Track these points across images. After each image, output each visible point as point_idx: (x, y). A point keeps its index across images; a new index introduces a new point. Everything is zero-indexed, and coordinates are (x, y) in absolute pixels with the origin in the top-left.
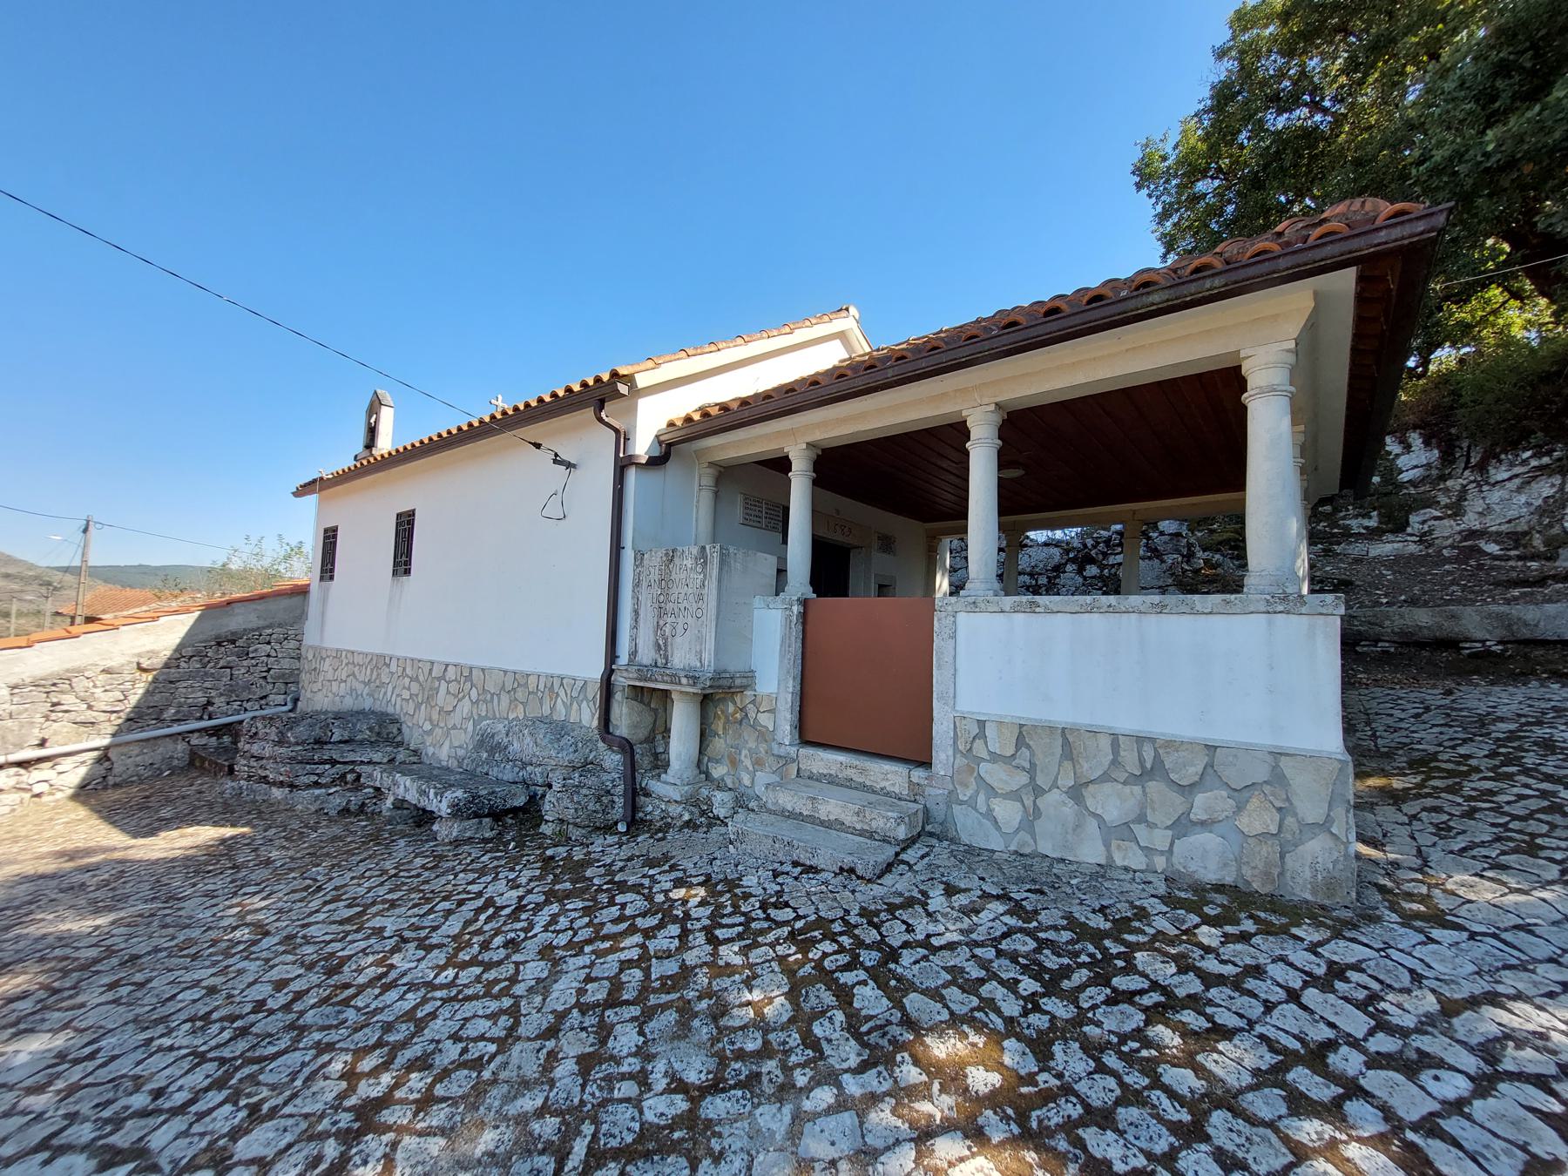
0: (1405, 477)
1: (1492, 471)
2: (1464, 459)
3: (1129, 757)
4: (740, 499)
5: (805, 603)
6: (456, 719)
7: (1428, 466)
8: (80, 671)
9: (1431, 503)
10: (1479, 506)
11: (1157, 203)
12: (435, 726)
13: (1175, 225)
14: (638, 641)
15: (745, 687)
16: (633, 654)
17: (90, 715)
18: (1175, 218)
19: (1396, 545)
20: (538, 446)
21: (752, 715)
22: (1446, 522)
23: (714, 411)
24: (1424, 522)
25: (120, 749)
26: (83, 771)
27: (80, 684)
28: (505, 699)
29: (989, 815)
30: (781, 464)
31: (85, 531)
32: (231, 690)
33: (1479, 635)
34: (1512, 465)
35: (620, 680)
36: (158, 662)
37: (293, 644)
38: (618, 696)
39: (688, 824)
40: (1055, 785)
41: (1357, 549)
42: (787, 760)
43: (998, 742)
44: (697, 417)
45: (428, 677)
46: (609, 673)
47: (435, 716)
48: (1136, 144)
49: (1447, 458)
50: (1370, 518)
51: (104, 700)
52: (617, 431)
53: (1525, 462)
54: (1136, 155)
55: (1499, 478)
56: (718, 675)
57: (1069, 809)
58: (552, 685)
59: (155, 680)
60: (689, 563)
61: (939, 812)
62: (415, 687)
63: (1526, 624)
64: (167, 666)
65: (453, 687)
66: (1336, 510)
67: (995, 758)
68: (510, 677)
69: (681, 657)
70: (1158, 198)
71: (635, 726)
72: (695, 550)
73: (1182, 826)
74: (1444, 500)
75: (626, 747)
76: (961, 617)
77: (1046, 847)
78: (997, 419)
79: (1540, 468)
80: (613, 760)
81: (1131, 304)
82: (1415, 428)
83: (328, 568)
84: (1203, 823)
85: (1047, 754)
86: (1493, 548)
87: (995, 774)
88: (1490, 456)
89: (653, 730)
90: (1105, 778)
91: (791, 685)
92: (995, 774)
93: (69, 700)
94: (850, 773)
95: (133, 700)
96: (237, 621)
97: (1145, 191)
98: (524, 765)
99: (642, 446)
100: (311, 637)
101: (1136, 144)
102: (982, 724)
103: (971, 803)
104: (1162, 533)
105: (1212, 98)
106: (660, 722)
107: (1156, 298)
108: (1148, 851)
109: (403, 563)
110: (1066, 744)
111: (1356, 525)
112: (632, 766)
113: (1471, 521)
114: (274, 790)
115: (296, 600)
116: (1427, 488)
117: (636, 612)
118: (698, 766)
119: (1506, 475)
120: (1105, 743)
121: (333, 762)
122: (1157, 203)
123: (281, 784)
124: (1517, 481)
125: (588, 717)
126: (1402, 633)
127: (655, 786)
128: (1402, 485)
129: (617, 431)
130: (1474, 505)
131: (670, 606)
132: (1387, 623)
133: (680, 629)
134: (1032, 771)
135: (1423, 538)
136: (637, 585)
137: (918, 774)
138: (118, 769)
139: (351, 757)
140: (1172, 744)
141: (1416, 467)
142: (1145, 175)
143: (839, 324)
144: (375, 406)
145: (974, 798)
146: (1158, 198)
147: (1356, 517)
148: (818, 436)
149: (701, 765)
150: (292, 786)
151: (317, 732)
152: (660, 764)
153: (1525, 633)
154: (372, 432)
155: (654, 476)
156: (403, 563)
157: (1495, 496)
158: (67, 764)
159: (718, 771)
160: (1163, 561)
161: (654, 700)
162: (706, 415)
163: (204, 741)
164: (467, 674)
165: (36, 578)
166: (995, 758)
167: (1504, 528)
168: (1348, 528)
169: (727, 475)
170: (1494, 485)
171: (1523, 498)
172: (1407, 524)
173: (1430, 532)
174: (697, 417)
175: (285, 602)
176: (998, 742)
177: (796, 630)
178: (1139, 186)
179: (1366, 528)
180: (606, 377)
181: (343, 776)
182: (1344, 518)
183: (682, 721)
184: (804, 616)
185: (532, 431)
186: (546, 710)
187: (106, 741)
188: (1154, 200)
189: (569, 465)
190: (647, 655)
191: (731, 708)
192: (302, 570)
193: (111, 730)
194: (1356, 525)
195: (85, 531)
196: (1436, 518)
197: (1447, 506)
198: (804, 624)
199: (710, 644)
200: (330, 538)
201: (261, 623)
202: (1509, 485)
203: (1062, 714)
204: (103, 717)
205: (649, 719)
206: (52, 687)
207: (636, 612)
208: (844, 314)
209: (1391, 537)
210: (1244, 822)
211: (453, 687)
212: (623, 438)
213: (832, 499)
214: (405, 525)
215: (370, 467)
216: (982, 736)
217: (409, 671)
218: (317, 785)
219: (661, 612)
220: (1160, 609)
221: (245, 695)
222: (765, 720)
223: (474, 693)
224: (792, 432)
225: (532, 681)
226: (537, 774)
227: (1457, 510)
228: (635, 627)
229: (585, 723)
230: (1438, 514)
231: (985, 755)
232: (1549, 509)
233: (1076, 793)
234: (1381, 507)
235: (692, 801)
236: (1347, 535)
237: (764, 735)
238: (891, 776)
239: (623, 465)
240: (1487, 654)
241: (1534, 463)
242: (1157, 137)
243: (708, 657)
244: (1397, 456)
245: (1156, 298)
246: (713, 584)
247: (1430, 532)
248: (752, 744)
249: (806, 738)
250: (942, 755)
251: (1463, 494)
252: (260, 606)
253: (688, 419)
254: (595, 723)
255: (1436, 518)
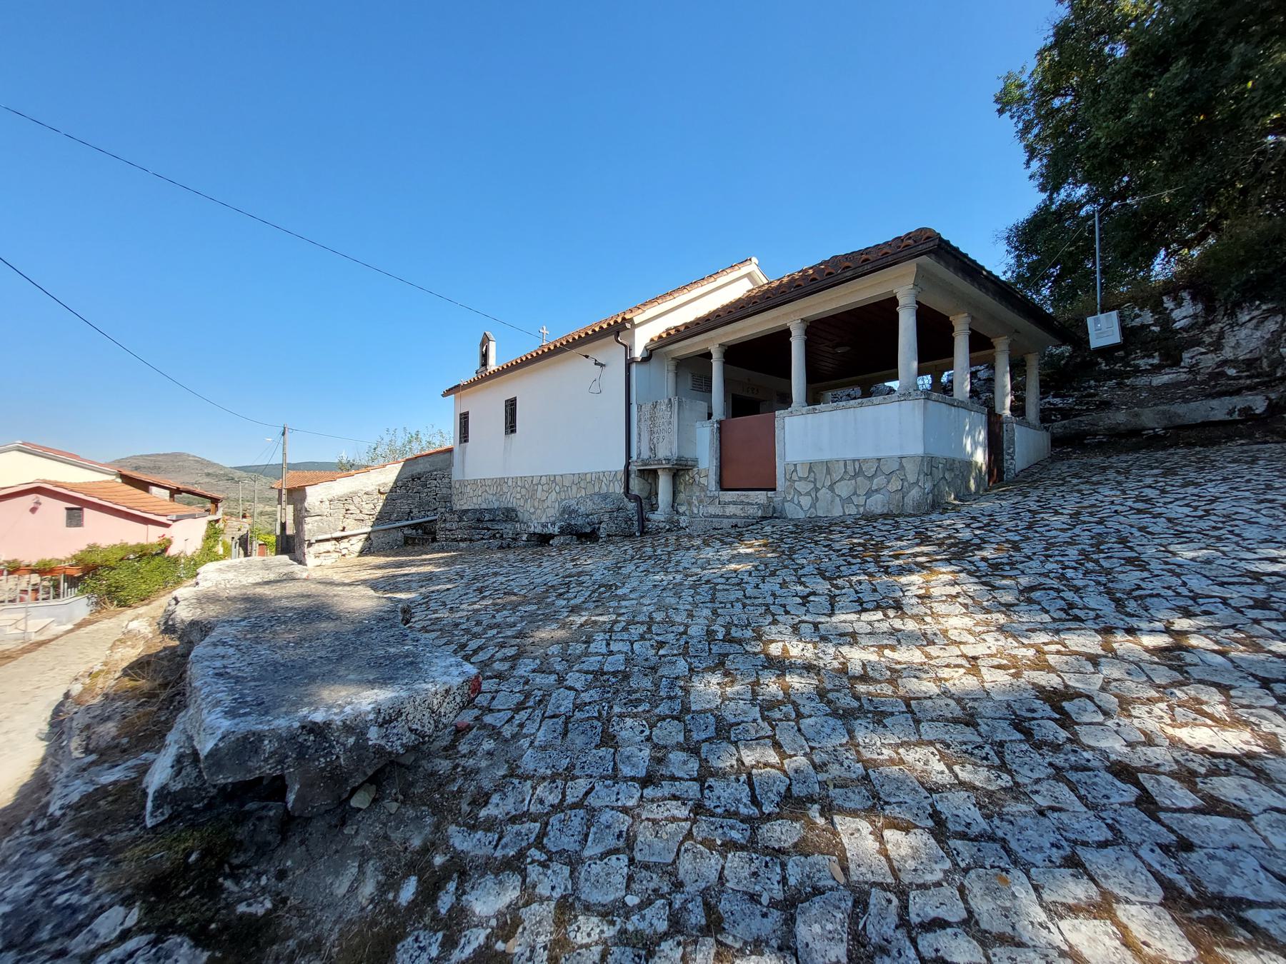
0: (1178, 325)
1: (1240, 316)
2: (1223, 308)
3: (850, 468)
4: (690, 375)
5: (720, 422)
6: (549, 503)
7: (1195, 316)
8: (356, 493)
9: (1199, 343)
10: (1232, 342)
11: (1018, 122)
12: (536, 509)
13: (1035, 136)
14: (641, 449)
15: (694, 466)
16: (639, 455)
17: (361, 516)
18: (1035, 131)
19: (1171, 376)
20: (587, 357)
21: (697, 479)
22: (1209, 356)
23: (673, 332)
24: (1192, 358)
25: (376, 534)
26: (361, 544)
27: (356, 500)
28: (574, 488)
29: (799, 504)
30: (708, 355)
31: (283, 434)
32: (420, 505)
33: (1151, 425)
34: (1250, 311)
35: (633, 468)
36: (387, 489)
37: (447, 480)
38: (633, 476)
39: (668, 530)
40: (823, 486)
41: (1142, 381)
42: (714, 498)
43: (802, 472)
44: (664, 335)
45: (530, 486)
46: (628, 465)
47: (536, 504)
48: (999, 78)
49: (1210, 310)
50: (1154, 357)
51: (367, 508)
52: (625, 346)
53: (1258, 308)
54: (998, 87)
55: (1244, 320)
56: (679, 459)
57: (830, 494)
58: (599, 477)
59: (387, 499)
60: (664, 407)
61: (779, 507)
62: (524, 491)
63: (1179, 416)
64: (391, 491)
65: (546, 488)
66: (1128, 354)
67: (801, 479)
68: (577, 476)
69: (662, 453)
70: (1019, 117)
71: (641, 490)
72: (666, 401)
73: (869, 494)
74: (1207, 340)
75: (637, 499)
76: (787, 419)
77: (820, 513)
78: (803, 326)
79: (1268, 310)
80: (632, 506)
81: (840, 277)
82: (1184, 288)
83: (464, 436)
84: (876, 490)
85: (820, 473)
86: (1232, 372)
87: (801, 486)
88: (1238, 305)
89: (650, 493)
90: (842, 479)
91: (715, 463)
92: (801, 486)
93: (352, 507)
94: (742, 498)
95: (379, 508)
96: (419, 468)
97: (1008, 114)
98: (588, 516)
99: (638, 353)
100: (456, 475)
101: (999, 78)
102: (795, 465)
103: (792, 501)
104: (980, 380)
105: (1054, 35)
106: (653, 490)
107: (848, 274)
108: (857, 506)
109: (511, 427)
110: (828, 468)
111: (1143, 363)
112: (641, 511)
113: (1228, 353)
114: (461, 544)
115: (447, 455)
116: (1197, 332)
117: (640, 434)
118: (673, 506)
119: (1247, 318)
120: (842, 464)
121: (489, 529)
122: (1018, 122)
123: (465, 540)
124: (1254, 321)
125: (619, 489)
126: (1109, 429)
127: (652, 516)
128: (1177, 331)
129: (625, 346)
130: (1230, 341)
131: (655, 429)
132: (1101, 423)
133: (661, 440)
134: (815, 482)
135: (1192, 369)
136: (639, 421)
137: (770, 493)
138: (375, 544)
139: (496, 527)
140: (866, 460)
141: (1185, 317)
142: (1004, 103)
143: (745, 269)
144: (485, 341)
145: (793, 498)
146: (1019, 117)
147: (1143, 358)
148: (724, 340)
149: (674, 504)
150: (471, 540)
151: (478, 515)
152: (654, 508)
153: (1179, 421)
154: (485, 356)
155: (645, 367)
156: (511, 427)
157: (1243, 333)
158: (354, 540)
159: (682, 509)
160: (979, 399)
161: (650, 475)
162: (669, 334)
163: (410, 532)
164: (553, 480)
165: (225, 475)
166: (801, 479)
167: (1248, 356)
168: (1137, 366)
169: (682, 364)
170: (1241, 326)
171: (1258, 334)
172: (1181, 360)
173: (1197, 364)
174: (664, 335)
175: (442, 457)
176: (802, 472)
177: (716, 435)
178: (1001, 112)
179: (1151, 365)
180: (619, 320)
181: (494, 535)
182: (1134, 359)
183: (664, 484)
184: (720, 430)
185: (583, 349)
186: (597, 489)
187: (369, 529)
188: (1016, 119)
189: (602, 365)
190: (646, 454)
191: (687, 478)
192: (449, 439)
193: (371, 524)
194: (1143, 363)
195: (283, 434)
196: (1202, 354)
197: (1210, 344)
198: (720, 433)
199: (675, 444)
200: (464, 418)
201: (432, 468)
202: (1249, 325)
203: (826, 456)
204: (367, 517)
205: (648, 487)
206: (347, 499)
207: (640, 434)
208: (748, 262)
209: (1167, 370)
210: (889, 487)
211: (546, 488)
212: (628, 349)
213: (742, 373)
214: (511, 406)
215: (485, 378)
216: (795, 470)
217: (519, 483)
218: (482, 539)
219: (652, 432)
220: (861, 405)
221: (427, 508)
222: (703, 481)
223: (557, 488)
224: (711, 339)
225: (588, 477)
226: (595, 518)
227: (1217, 346)
228: (639, 441)
229: (617, 491)
230: (1203, 350)
231: (796, 478)
232: (1274, 341)
233: (831, 488)
234: (1161, 348)
235: (670, 521)
236: (1137, 371)
237: (704, 488)
238: (760, 497)
239: (629, 363)
240: (1156, 436)
241: (1264, 307)
242: (1016, 70)
243: (675, 450)
244: (1172, 310)
245: (848, 274)
246: (675, 420)
247: (1197, 364)
248: (698, 494)
249: (723, 487)
250: (780, 483)
251: (1221, 335)
252: (430, 459)
253: (660, 337)
254: (622, 491)
255: (1202, 354)
